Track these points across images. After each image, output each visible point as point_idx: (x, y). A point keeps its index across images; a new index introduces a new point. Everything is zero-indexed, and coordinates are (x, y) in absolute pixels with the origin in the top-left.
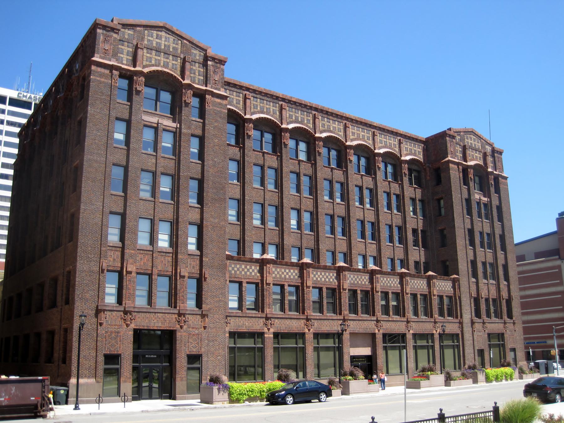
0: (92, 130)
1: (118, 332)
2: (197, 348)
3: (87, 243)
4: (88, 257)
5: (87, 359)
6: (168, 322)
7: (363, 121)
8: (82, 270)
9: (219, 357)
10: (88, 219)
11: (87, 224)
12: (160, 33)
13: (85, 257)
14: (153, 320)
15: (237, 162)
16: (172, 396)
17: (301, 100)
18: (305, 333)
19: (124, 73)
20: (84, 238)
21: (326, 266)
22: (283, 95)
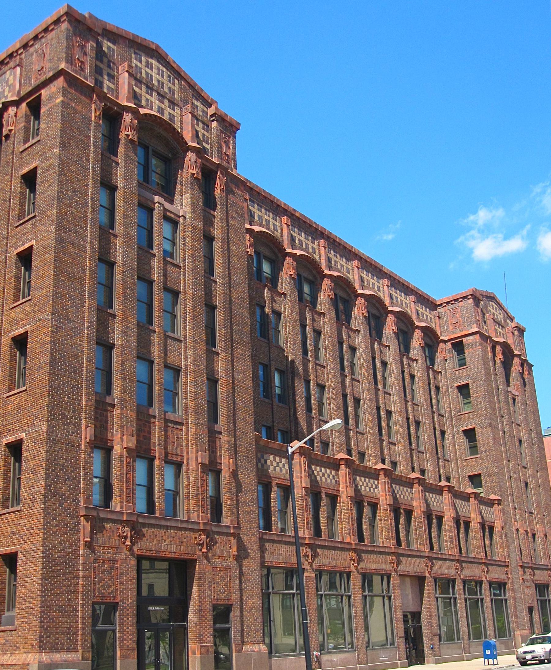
0: (65, 190)
1: (115, 561)
2: (226, 593)
3: (62, 389)
4: (65, 416)
5: (65, 613)
6: (185, 544)
7: (374, 263)
8: (55, 440)
9: (253, 611)
10: (64, 345)
11: (61, 354)
12: (151, 60)
13: (60, 415)
14: (165, 541)
15: (147, 363)
16: (422, 662)
17: (306, 218)
18: (351, 572)
19: (109, 107)
20: (57, 380)
21: (184, 531)
22: (285, 204)
